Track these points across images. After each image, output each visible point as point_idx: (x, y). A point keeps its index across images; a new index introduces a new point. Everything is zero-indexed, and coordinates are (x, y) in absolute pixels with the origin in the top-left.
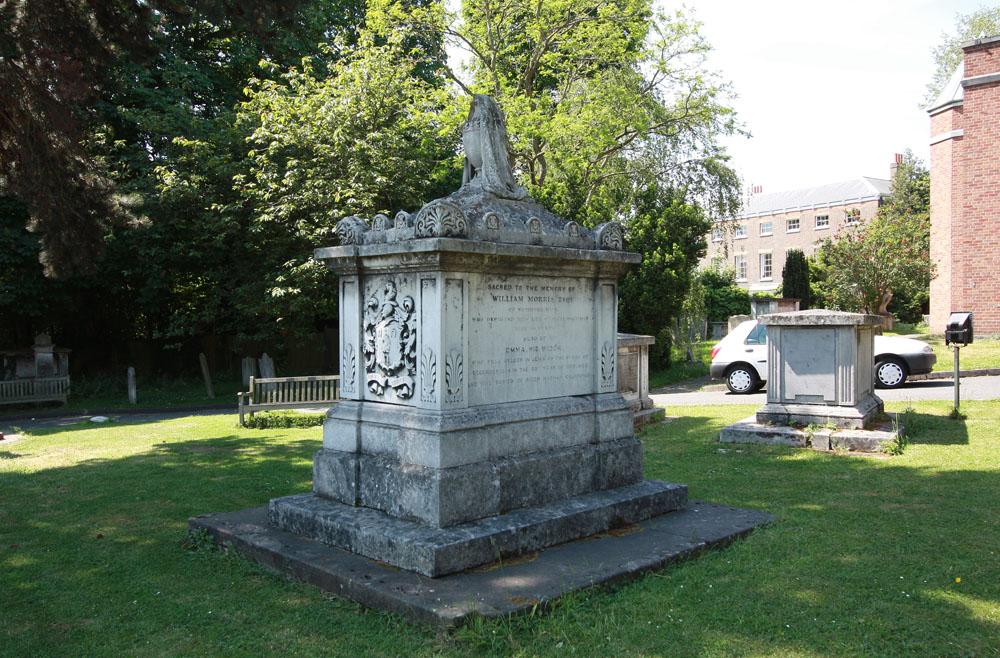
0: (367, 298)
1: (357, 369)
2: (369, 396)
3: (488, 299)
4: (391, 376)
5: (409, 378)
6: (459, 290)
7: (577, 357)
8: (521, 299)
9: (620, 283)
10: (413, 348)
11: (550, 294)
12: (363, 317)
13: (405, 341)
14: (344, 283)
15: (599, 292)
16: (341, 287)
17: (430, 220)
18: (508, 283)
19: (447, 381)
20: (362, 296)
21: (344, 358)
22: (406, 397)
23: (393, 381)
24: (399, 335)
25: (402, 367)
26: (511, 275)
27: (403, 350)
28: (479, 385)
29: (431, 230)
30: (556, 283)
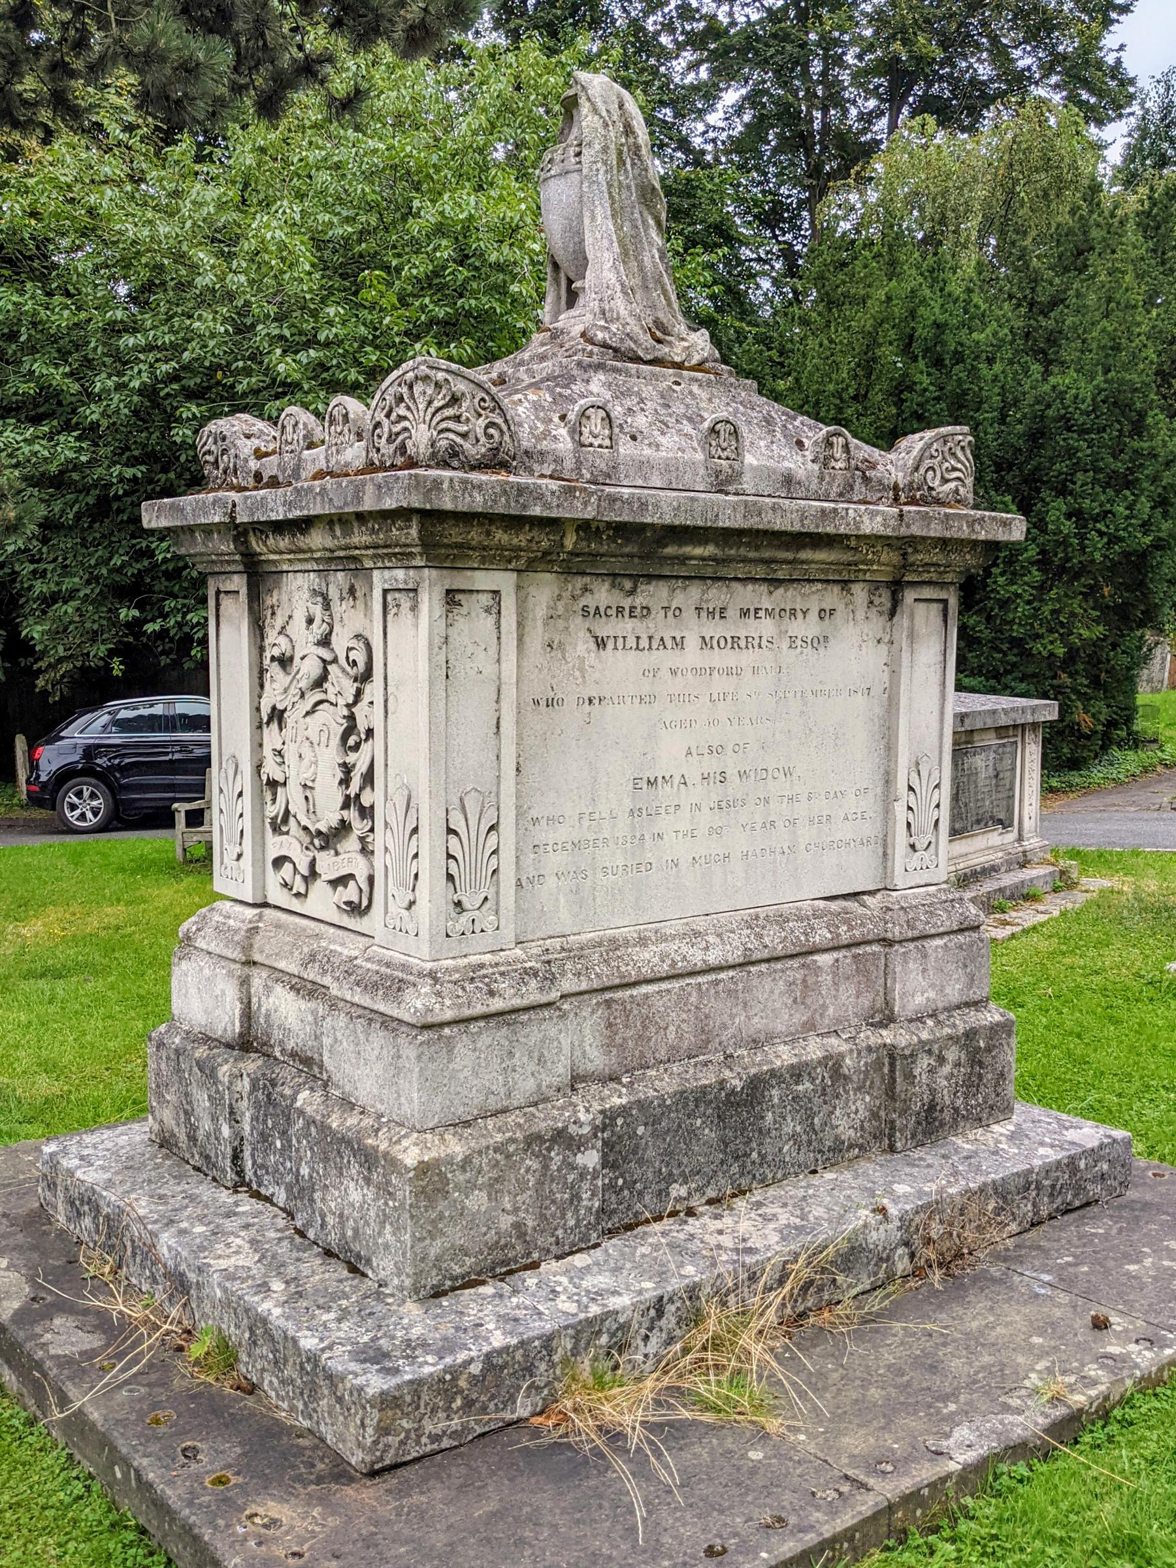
0: (272, 636)
1: (247, 823)
2: (277, 896)
3: (582, 646)
4: (322, 848)
5: (361, 860)
6: (491, 620)
7: (839, 795)
8: (679, 643)
9: (968, 603)
10: (369, 778)
11: (766, 627)
12: (262, 686)
13: (351, 758)
14: (218, 592)
15: (902, 620)
16: (211, 603)
17: (402, 418)
18: (639, 600)
19: (450, 877)
20: (258, 628)
21: (221, 791)
22: (356, 909)
23: (329, 866)
24: (336, 740)
25: (345, 826)
26: (650, 578)
27: (345, 782)
28: (551, 882)
29: (402, 449)
30: (785, 597)
